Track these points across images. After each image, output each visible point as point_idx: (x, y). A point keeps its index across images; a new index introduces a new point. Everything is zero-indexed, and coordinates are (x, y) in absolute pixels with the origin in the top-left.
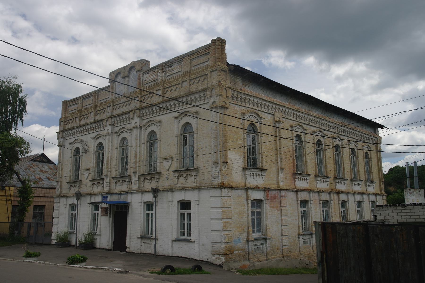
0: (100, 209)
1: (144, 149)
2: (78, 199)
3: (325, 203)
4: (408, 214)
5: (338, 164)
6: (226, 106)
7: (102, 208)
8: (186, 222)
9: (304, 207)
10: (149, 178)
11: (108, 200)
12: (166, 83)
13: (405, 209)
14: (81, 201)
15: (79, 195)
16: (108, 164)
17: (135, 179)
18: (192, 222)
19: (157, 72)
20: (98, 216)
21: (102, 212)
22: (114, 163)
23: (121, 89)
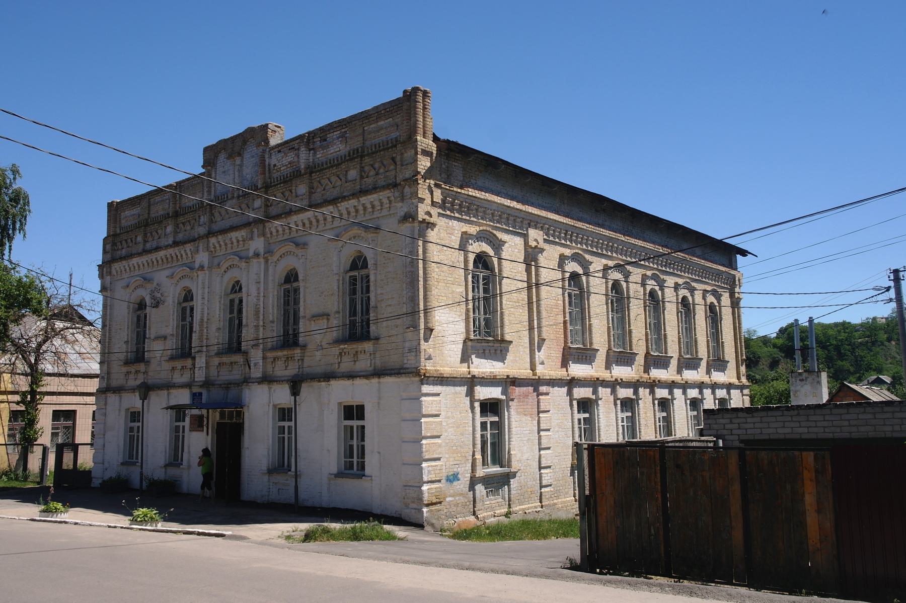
0: (187, 419)
1: (273, 301)
2: (144, 398)
3: (628, 405)
4: (757, 425)
5: (657, 327)
6: (432, 220)
7: (192, 416)
8: (355, 442)
9: (584, 412)
10: (133, 371)
11: (204, 401)
12: (316, 172)
13: (753, 417)
14: (149, 403)
15: (146, 390)
16: (201, 331)
17: (256, 355)
18: (367, 443)
19: (298, 149)
20: (183, 432)
21: (191, 424)
22: (213, 328)
23: (227, 178)
